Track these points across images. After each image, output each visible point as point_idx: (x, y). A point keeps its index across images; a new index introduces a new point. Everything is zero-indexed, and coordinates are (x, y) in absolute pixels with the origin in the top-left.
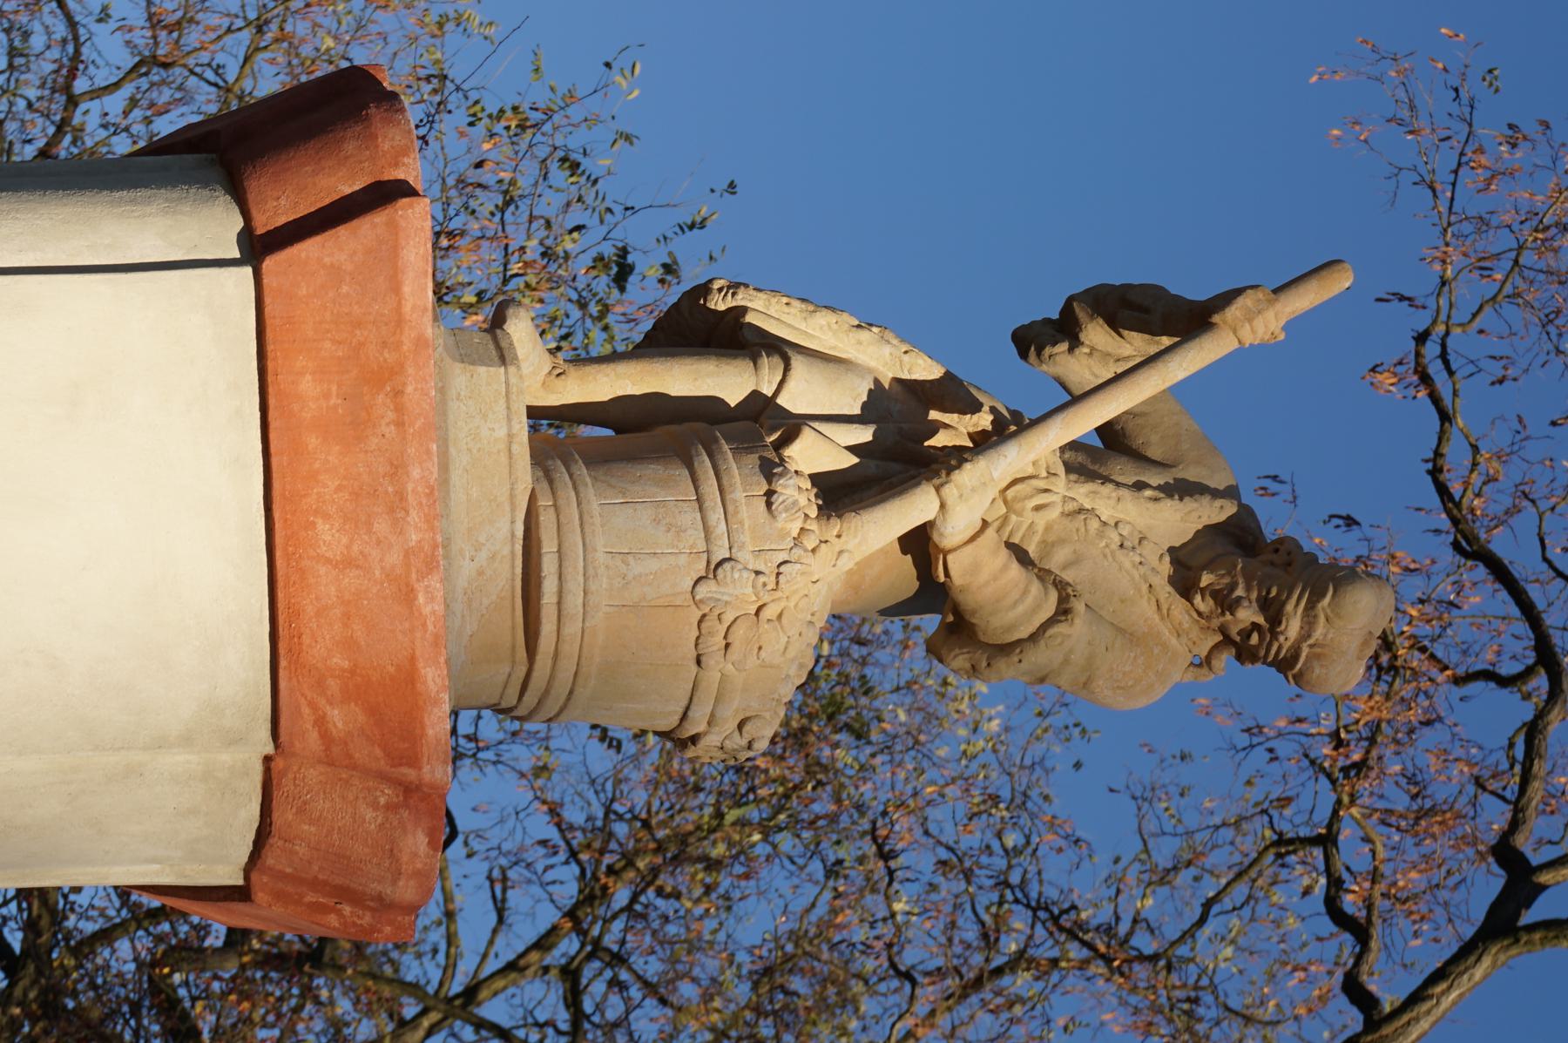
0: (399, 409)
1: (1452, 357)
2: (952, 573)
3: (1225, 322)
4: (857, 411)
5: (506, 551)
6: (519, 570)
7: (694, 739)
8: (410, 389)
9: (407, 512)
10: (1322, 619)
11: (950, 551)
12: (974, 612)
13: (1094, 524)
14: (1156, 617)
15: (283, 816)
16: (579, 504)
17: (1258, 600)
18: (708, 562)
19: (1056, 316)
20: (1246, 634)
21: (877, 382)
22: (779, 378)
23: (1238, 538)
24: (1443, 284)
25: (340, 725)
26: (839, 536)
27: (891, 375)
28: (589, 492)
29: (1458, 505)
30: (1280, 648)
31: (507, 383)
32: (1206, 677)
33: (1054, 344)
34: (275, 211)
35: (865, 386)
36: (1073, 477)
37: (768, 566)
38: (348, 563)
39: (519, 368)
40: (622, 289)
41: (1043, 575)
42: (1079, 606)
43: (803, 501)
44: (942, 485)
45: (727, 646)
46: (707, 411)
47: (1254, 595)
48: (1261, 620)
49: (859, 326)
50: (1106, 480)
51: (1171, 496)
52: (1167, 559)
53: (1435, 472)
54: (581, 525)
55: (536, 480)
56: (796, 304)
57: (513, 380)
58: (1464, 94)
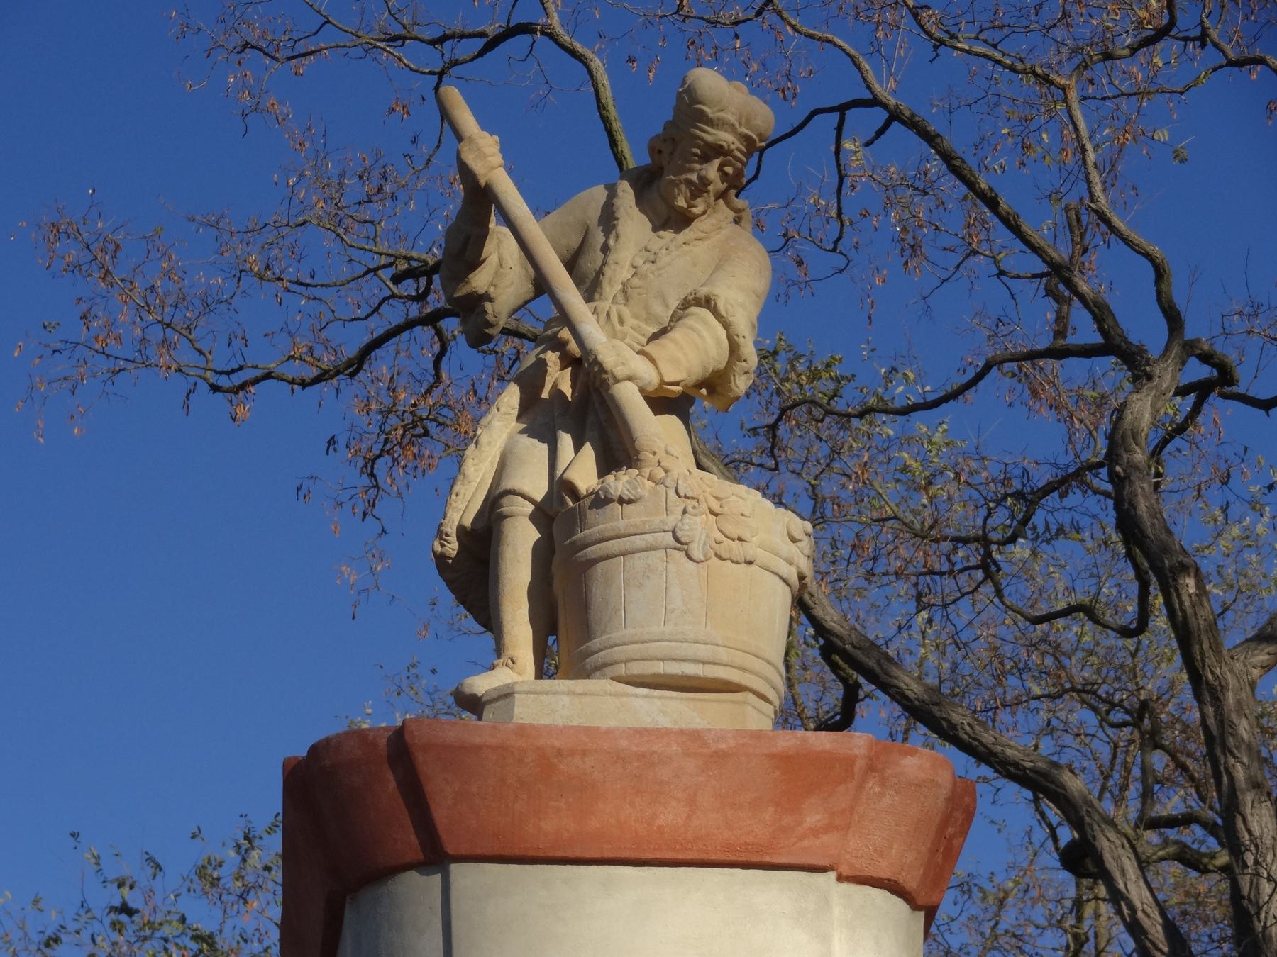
0: (572, 753)
1: (229, 368)
2: (678, 378)
3: (485, 175)
4: (545, 446)
5: (659, 703)
6: (674, 694)
7: (801, 577)
8: (557, 744)
9: (654, 752)
10: (721, 114)
11: (662, 379)
12: (705, 368)
13: (636, 281)
14: (707, 242)
15: (884, 872)
16: (625, 644)
17: (701, 164)
18: (675, 549)
20: (724, 175)
21: (522, 432)
22: (520, 499)
23: (647, 183)
24: (180, 370)
25: (819, 817)
26: (654, 453)
27: (514, 424)
28: (615, 636)
29: (326, 372)
30: (739, 150)
31: (528, 693)
32: (747, 216)
33: (486, 313)
34: (407, 840)
35: (526, 440)
36: (597, 296)
37: (678, 505)
38: (692, 802)
39: (515, 683)
40: (137, 911)
41: (676, 318)
42: (703, 292)
43: (626, 478)
44: (614, 377)
45: (740, 539)
46: (543, 555)
47: (697, 166)
48: (717, 162)
49: (476, 443)
50: (600, 272)
51: (614, 227)
52: (661, 233)
53: (304, 384)
55: (604, 677)
56: (456, 488)
57: (525, 688)
58: (58, 346)
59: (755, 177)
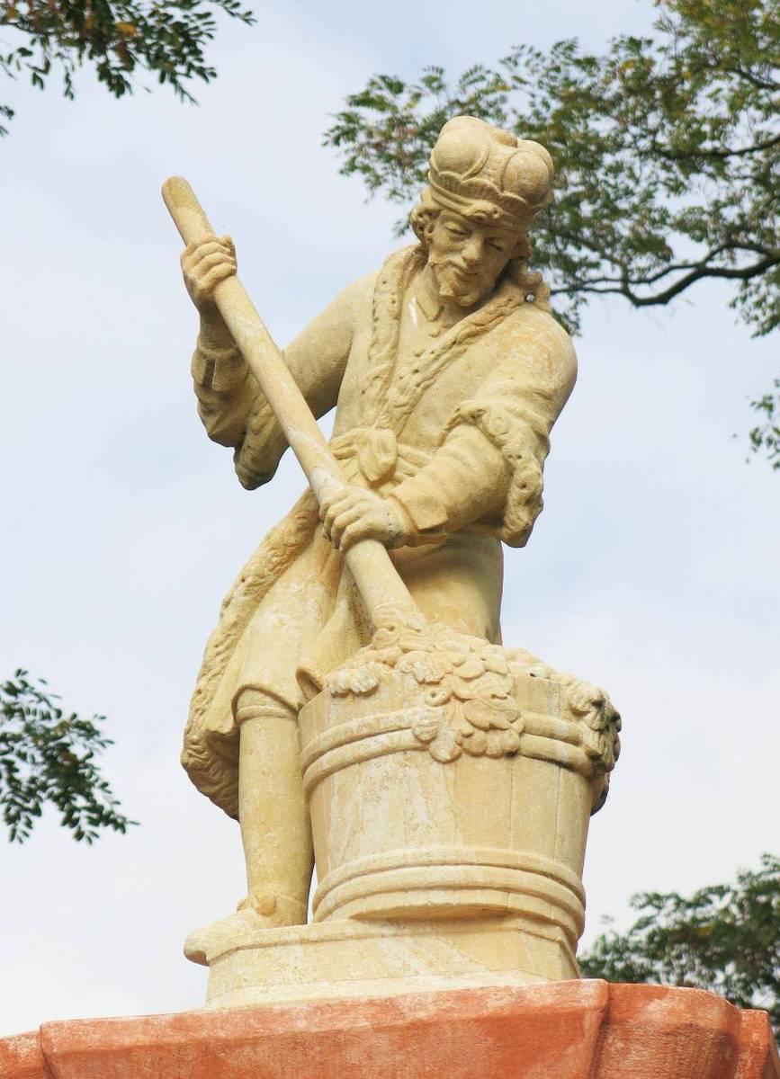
0: (240, 1043)
9: (339, 1031)
19: (232, 450)
54: (382, 870)
59: (664, 299)
